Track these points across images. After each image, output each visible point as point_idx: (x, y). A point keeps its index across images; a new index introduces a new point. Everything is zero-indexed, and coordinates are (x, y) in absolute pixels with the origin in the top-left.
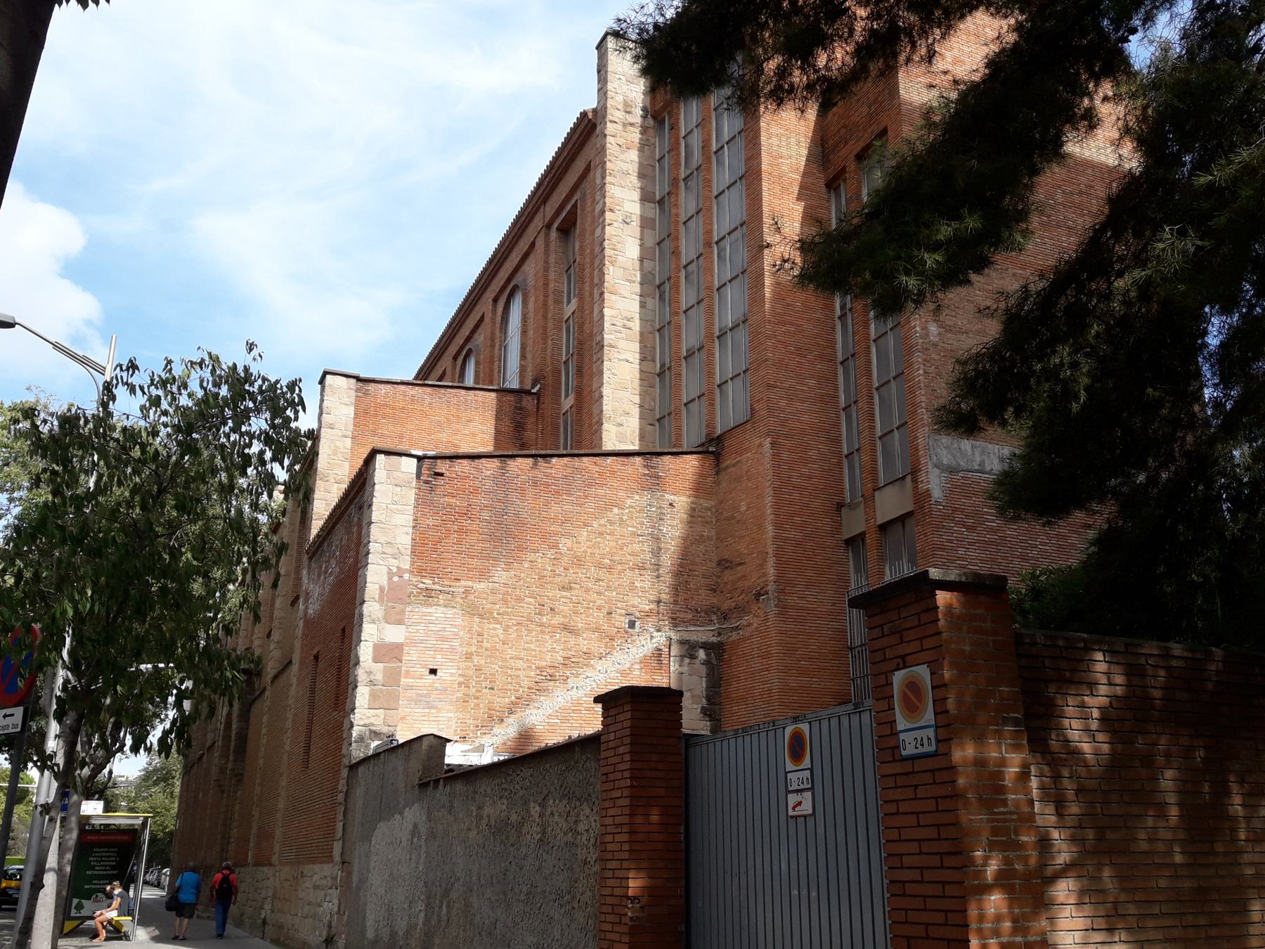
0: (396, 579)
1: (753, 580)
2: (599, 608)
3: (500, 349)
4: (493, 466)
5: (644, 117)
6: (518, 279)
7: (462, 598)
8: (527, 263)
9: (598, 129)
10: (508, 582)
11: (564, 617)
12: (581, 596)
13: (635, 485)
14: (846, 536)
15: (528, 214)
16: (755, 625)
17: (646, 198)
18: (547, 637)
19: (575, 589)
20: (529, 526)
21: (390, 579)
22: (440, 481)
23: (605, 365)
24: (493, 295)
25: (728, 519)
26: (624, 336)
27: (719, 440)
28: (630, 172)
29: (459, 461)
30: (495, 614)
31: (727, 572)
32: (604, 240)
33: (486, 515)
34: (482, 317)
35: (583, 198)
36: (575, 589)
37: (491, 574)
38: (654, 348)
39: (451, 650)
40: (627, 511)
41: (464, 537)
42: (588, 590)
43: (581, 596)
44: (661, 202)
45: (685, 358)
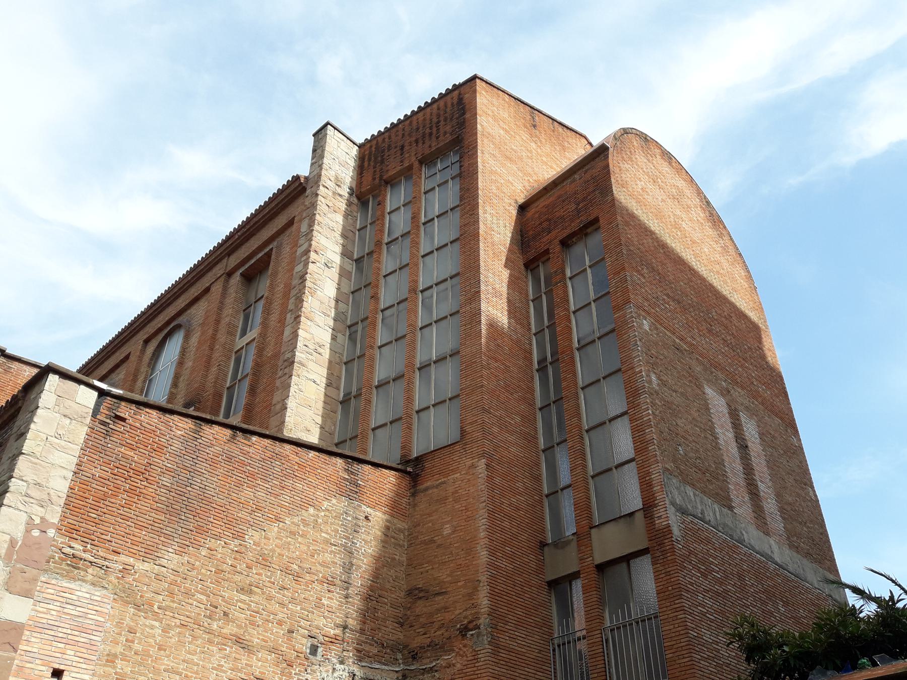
0: (36, 533)
1: (457, 612)
2: (280, 623)
3: (144, 381)
4: (185, 426)
5: (351, 194)
6: (181, 320)
7: (118, 578)
8: (195, 307)
9: (307, 192)
10: (178, 570)
11: (239, 627)
12: (262, 604)
13: (333, 488)
14: (551, 577)
15: (209, 264)
16: (458, 666)
17: (346, 254)
18: (215, 648)
19: (255, 593)
20: (214, 506)
21: (28, 531)
22: (119, 427)
23: (293, 380)
24: (145, 337)
25: (424, 543)
26: (314, 358)
27: (419, 460)
28: (335, 229)
29: (147, 410)
30: (156, 607)
31: (420, 602)
32: (307, 273)
33: (166, 480)
34: (127, 357)
35: (279, 247)
36: (255, 593)
37: (159, 555)
38: (339, 378)
39: (88, 646)
40: (323, 514)
41: (135, 500)
42: (269, 598)
43: (262, 604)
44: (358, 261)
45: (377, 387)
